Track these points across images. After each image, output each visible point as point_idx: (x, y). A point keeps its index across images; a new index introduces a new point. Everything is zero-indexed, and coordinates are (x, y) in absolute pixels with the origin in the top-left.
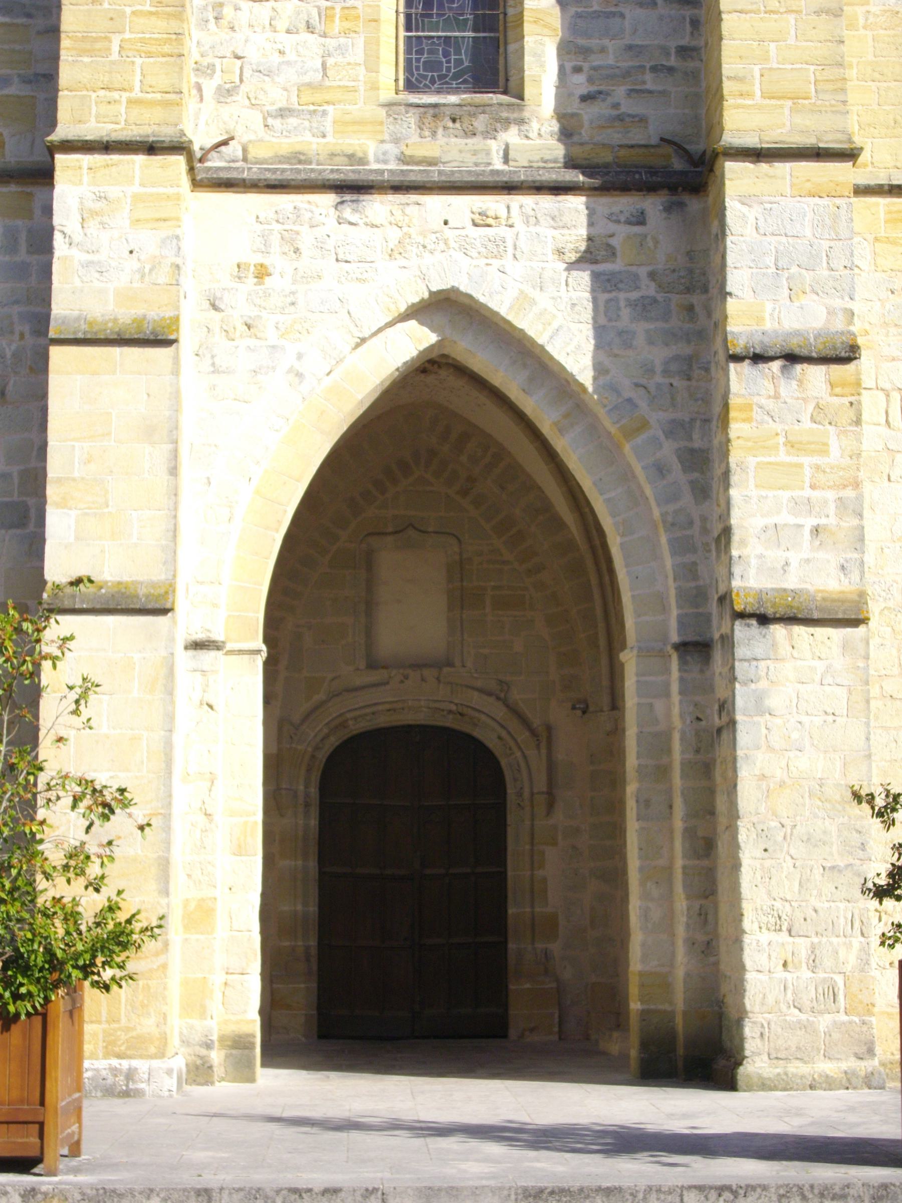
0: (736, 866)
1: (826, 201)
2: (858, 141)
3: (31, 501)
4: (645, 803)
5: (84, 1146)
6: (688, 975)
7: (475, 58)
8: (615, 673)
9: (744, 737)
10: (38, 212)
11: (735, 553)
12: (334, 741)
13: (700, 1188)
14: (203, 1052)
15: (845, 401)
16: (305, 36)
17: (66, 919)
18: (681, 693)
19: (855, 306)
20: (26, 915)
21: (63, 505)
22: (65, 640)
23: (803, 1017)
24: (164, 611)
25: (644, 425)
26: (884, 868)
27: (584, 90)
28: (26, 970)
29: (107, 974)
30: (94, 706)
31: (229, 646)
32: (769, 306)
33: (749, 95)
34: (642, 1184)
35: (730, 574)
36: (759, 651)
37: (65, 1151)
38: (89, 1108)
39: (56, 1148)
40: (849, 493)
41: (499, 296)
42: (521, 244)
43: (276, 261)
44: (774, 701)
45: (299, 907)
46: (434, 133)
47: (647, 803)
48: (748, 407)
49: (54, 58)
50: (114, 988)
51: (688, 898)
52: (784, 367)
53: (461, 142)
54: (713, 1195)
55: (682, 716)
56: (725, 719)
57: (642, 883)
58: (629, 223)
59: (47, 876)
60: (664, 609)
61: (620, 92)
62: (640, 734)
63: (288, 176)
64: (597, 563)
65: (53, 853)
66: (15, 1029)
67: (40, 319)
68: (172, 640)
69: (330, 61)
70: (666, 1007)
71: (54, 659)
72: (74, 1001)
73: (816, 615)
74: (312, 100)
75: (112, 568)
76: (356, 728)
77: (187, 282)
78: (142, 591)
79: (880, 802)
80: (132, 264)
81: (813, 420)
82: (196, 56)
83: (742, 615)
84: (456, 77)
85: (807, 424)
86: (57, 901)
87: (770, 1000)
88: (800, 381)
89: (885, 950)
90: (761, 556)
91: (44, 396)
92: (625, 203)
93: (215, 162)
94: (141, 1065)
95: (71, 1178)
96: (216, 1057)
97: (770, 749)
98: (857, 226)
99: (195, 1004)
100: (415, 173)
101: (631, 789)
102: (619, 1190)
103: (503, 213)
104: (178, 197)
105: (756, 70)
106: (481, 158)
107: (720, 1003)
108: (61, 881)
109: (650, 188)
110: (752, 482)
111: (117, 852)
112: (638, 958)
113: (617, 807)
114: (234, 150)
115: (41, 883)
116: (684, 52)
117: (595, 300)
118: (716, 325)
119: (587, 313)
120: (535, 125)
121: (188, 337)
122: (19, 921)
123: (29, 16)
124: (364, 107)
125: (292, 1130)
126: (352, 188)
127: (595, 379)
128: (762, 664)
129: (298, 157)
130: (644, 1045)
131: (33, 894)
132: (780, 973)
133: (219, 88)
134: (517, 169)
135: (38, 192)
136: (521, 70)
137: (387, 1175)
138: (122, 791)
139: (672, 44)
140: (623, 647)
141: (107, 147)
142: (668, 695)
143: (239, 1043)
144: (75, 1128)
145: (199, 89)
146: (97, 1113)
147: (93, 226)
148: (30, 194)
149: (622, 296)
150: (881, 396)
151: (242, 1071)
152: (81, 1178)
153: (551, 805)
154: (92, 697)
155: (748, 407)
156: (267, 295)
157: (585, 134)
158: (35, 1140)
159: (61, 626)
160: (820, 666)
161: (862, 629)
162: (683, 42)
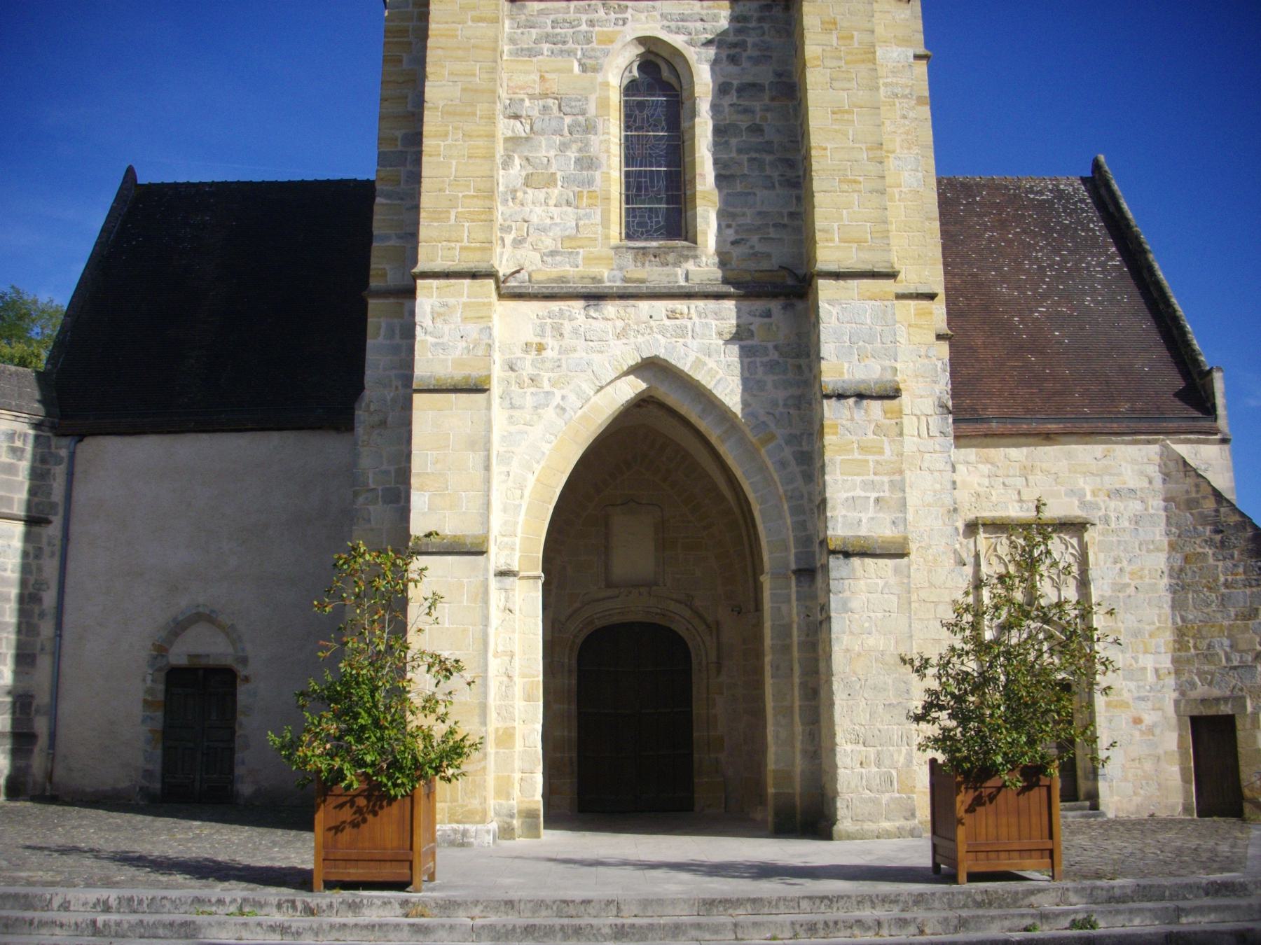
0: (832, 704)
1: (878, 303)
2: (897, 267)
3: (402, 487)
4: (776, 668)
5: (437, 875)
6: (803, 772)
7: (667, 220)
8: (758, 588)
9: (836, 626)
10: (406, 314)
11: (829, 514)
12: (586, 632)
13: (810, 898)
14: (509, 820)
15: (894, 422)
16: (565, 208)
17: (424, 739)
18: (798, 600)
19: (898, 366)
20: (400, 736)
21: (421, 489)
22: (422, 570)
23: (872, 795)
24: (482, 553)
25: (772, 437)
26: (920, 704)
27: (732, 238)
28: (401, 769)
29: (450, 772)
30: (442, 610)
31: (522, 574)
32: (846, 365)
33: (832, 240)
34: (775, 896)
35: (826, 527)
36: (844, 574)
37: (425, 878)
38: (439, 853)
39: (420, 877)
40: (897, 477)
41: (685, 358)
42: (697, 329)
43: (549, 341)
44: (854, 604)
45: (566, 733)
46: (643, 265)
47: (778, 668)
48: (835, 426)
49: (416, 223)
50: (454, 780)
51: (803, 724)
52: (856, 402)
53: (660, 269)
54: (818, 902)
55: (798, 614)
56: (824, 615)
57: (775, 716)
58: (761, 316)
59: (413, 713)
60: (787, 549)
61: (755, 239)
62: (773, 627)
63: (556, 290)
64: (745, 521)
65: (416, 700)
66: (395, 805)
67: (408, 378)
68: (487, 570)
69: (581, 223)
70: (790, 791)
71: (416, 582)
72: (430, 788)
73: (878, 552)
74: (571, 243)
75: (450, 526)
76: (599, 624)
77: (497, 356)
78: (468, 541)
79: (917, 663)
80: (462, 344)
81: (874, 434)
82: (500, 220)
83: (834, 552)
84: (656, 231)
85: (871, 436)
86: (419, 728)
87: (853, 785)
88: (866, 411)
89: (920, 753)
90: (845, 516)
91: (409, 423)
92: (759, 305)
93: (512, 283)
94: (471, 828)
95: (429, 894)
96: (516, 823)
97: (852, 633)
98: (898, 318)
99: (504, 790)
100: (632, 287)
101: (768, 659)
102: (761, 899)
103: (686, 311)
104: (490, 304)
105: (836, 226)
106: (672, 279)
107: (823, 795)
108: (421, 716)
109: (774, 296)
110: (838, 471)
111: (455, 699)
112: (773, 760)
113: (758, 671)
114: (524, 275)
115: (409, 717)
116: (792, 215)
117: (742, 363)
118: (815, 377)
119: (737, 370)
120: (704, 259)
121: (496, 389)
122: (396, 740)
123: (402, 199)
124: (599, 249)
125: (562, 867)
126: (594, 297)
127: (743, 409)
128: (846, 582)
129: (562, 279)
130: (777, 814)
131: (405, 724)
132: (858, 769)
133: (514, 239)
134: (694, 284)
135: (407, 303)
136: (695, 227)
137: (620, 892)
138: (457, 661)
139: (785, 211)
140: (762, 572)
141: (447, 275)
142: (789, 601)
143: (530, 815)
144: (431, 864)
145: (503, 240)
146: (444, 856)
147: (439, 324)
148: (402, 304)
149: (758, 360)
150: (915, 418)
151: (532, 831)
152: (435, 894)
153: (719, 672)
154: (439, 605)
155: (835, 426)
156: (543, 361)
157: (734, 263)
158: (408, 871)
159: (418, 563)
160: (881, 582)
161: (906, 560)
162: (793, 210)
